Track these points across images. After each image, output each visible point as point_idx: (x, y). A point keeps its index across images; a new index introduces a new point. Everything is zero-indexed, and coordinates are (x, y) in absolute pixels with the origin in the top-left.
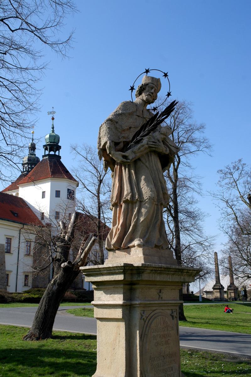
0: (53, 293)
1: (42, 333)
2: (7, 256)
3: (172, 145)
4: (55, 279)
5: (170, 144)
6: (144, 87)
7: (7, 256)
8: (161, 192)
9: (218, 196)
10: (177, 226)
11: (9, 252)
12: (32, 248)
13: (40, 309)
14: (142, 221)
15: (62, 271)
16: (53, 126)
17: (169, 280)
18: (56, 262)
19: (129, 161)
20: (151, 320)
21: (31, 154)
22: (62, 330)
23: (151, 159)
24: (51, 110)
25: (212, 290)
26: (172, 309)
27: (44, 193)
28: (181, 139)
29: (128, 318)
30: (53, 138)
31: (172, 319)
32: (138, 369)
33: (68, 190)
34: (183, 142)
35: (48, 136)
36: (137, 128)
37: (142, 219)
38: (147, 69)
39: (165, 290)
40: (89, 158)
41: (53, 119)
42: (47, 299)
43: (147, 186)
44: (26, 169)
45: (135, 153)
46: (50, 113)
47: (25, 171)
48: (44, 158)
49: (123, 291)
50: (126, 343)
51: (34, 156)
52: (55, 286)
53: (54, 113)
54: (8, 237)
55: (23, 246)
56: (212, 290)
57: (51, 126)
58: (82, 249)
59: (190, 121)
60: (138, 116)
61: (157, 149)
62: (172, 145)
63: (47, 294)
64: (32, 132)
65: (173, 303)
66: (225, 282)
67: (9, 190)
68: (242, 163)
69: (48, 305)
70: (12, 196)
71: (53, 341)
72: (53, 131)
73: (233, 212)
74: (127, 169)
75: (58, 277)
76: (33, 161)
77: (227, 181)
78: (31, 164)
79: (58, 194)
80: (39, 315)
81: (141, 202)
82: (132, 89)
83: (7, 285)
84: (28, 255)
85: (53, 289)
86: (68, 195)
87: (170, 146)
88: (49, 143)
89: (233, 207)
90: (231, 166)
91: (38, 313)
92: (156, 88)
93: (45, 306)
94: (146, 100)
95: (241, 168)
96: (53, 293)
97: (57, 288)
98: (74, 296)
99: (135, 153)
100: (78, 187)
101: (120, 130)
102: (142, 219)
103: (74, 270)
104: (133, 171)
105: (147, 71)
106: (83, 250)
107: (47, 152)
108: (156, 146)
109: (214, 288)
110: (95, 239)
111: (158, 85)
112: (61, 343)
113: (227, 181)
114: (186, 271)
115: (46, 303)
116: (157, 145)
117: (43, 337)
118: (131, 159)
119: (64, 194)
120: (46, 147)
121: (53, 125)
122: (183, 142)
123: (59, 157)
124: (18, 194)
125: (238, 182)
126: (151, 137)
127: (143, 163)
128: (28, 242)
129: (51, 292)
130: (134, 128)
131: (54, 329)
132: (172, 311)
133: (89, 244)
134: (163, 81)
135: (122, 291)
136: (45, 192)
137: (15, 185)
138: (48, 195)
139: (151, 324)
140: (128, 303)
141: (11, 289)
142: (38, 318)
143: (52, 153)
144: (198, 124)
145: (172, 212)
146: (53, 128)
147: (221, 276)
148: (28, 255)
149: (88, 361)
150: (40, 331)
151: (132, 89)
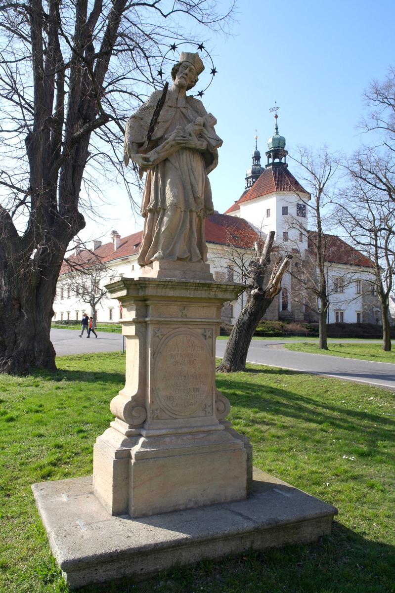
0: (244, 324)
3: (211, 137)
5: (209, 136)
6: (176, 68)
8: (191, 197)
13: (231, 340)
14: (163, 232)
15: (252, 299)
16: (277, 126)
17: (189, 296)
19: (151, 163)
21: (255, 165)
22: (255, 363)
23: (183, 157)
24: (273, 105)
27: (268, 210)
29: (141, 334)
30: (277, 142)
31: (204, 339)
32: (149, 386)
35: (271, 140)
36: (168, 121)
37: (163, 229)
38: (173, 45)
40: (305, 162)
41: (276, 117)
43: (171, 191)
44: (250, 183)
45: (158, 153)
46: (272, 110)
47: (249, 187)
49: (136, 307)
50: (139, 360)
51: (259, 167)
53: (277, 109)
57: (275, 127)
58: (274, 273)
60: (170, 107)
61: (187, 145)
62: (212, 137)
64: (255, 137)
69: (238, 336)
72: (277, 133)
74: (155, 173)
76: (256, 174)
78: (256, 177)
79: (285, 210)
81: (164, 210)
85: (244, 318)
86: (297, 211)
87: (208, 139)
88: (272, 149)
92: (193, 67)
93: (236, 337)
94: (179, 84)
98: (305, 330)
99: (158, 153)
100: (310, 199)
101: (145, 128)
102: (163, 229)
103: (265, 297)
104: (159, 175)
106: (275, 274)
107: (271, 161)
108: (185, 141)
110: (287, 261)
111: (195, 62)
114: (216, 286)
115: (237, 334)
116: (187, 140)
118: (152, 161)
119: (292, 211)
120: (269, 154)
121: (277, 125)
123: (285, 165)
126: (180, 131)
127: (172, 164)
130: (163, 122)
131: (247, 361)
132: (205, 330)
133: (281, 267)
134: (202, 54)
135: (135, 307)
136: (269, 209)
138: (273, 213)
140: (141, 320)
143: (277, 160)
146: (277, 129)
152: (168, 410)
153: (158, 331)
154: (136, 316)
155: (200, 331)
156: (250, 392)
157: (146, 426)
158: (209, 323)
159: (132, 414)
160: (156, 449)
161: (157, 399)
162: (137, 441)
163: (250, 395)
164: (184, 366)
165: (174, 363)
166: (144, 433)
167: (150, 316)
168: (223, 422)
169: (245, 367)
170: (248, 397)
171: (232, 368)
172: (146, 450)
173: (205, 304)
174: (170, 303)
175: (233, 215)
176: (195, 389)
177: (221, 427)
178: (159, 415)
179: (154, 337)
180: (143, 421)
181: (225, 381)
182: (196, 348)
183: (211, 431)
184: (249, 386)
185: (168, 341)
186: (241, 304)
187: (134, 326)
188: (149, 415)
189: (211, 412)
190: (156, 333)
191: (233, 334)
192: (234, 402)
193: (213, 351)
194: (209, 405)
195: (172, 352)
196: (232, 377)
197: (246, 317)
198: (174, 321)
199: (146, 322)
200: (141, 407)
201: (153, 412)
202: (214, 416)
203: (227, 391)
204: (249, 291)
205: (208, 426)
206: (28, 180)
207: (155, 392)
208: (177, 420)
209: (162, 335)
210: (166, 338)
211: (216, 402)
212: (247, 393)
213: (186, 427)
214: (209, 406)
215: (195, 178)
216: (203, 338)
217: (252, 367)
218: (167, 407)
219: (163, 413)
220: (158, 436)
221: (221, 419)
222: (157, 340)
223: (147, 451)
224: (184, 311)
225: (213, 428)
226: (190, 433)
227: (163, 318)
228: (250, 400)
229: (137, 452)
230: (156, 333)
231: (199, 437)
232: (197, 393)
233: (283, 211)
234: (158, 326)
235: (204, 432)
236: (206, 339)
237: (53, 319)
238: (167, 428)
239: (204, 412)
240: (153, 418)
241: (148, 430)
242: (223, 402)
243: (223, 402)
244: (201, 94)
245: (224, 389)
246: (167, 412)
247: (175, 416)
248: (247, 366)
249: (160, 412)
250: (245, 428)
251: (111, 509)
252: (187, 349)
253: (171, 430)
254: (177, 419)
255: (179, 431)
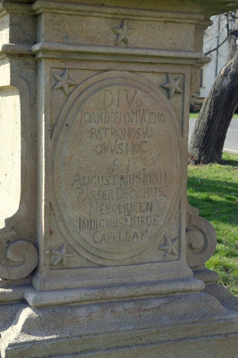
0: (223, 91)
1: (204, 154)
4: (227, 68)
18: (232, 36)
20: (84, 95)
26: (166, 73)
31: (164, 98)
32: (43, 198)
39: (142, 23)
42: (213, 100)
52: (227, 78)
63: (213, 93)
65: (168, 57)
71: (220, 168)
75: (231, 63)
80: (200, 126)
83: (201, 86)
85: (223, 84)
91: (198, 123)
93: (210, 112)
96: (222, 91)
97: (231, 82)
112: (232, 172)
115: (211, 107)
117: (205, 161)
129: (219, 90)
131: (225, 149)
132: (167, 77)
135: (7, 18)
139: (83, 102)
140: (22, 48)
142: (198, 132)
149: (228, 198)
150: (201, 151)
152: (83, 248)
153: (62, 76)
154: (11, 40)
155: (157, 79)
156: (233, 197)
157: (37, 282)
158: (177, 62)
159: (6, 256)
160: (54, 336)
161: (60, 225)
162: (15, 315)
163: (234, 202)
164: (118, 156)
165: (99, 150)
166: (30, 297)
167: (42, 39)
168: (202, 271)
169: (220, 157)
170: (231, 205)
171: (202, 158)
172: (33, 338)
173: (168, 15)
174: (88, 8)
176: (144, 207)
177: (198, 284)
178: (65, 259)
179: (52, 89)
180: (31, 271)
181: (193, 178)
182: (147, 117)
183: (175, 292)
184: (230, 188)
185: (86, 99)
186: (214, 67)
187: (8, 65)
188: (43, 259)
189: (176, 252)
190: (57, 81)
191: (205, 110)
192: (208, 213)
193: (185, 123)
194: (173, 237)
195: (94, 125)
196: (200, 172)
197: (227, 82)
198: (98, 54)
199: (33, 55)
200: (26, 243)
201: (51, 254)
202: (183, 259)
203: (196, 195)
204: (233, 40)
205: (170, 281)
207: (56, 212)
208: (104, 270)
209: (70, 85)
210: (81, 93)
211: (187, 231)
212: (228, 198)
213: (123, 285)
214: (173, 240)
215: (153, 72)
216: (162, 94)
217: (232, 158)
218: (81, 243)
219: (75, 254)
220: (61, 305)
221: (197, 267)
222: (61, 95)
223: (34, 342)
224: (120, 31)
225: (181, 286)
226: (131, 299)
227: (72, 44)
228: (234, 209)
229: (10, 346)
230: (57, 81)
231: (148, 307)
232: (148, 213)
234: (63, 65)
235: (161, 295)
236: (169, 98)
238: (82, 288)
239: (163, 252)
240: (51, 265)
241: (42, 291)
242: (201, 230)
243: (201, 230)
245: (192, 192)
246: (83, 253)
247: (99, 262)
248: (224, 157)
249: (68, 252)
250: (229, 259)
252: (127, 118)
253: (88, 293)
254: (103, 266)
255: (109, 293)
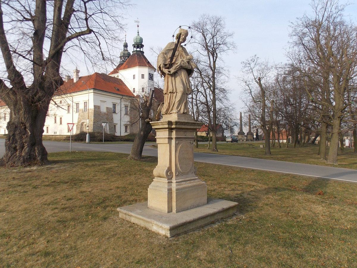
2: (114, 115)
7: (114, 115)
9: (241, 79)
10: (214, 97)
11: (114, 112)
12: (128, 109)
25: (237, 135)
27: (134, 76)
28: (219, 42)
33: (149, 74)
34: (220, 44)
46: (136, 22)
48: (134, 53)
54: (114, 103)
55: (124, 109)
56: (237, 135)
59: (225, 30)
66: (246, 130)
67: (112, 74)
68: (256, 57)
70: (114, 77)
73: (249, 89)
77: (247, 69)
79: (143, 76)
82: (173, 36)
84: (126, 114)
89: (249, 85)
90: (250, 59)
95: (256, 60)
105: (180, 27)
107: (135, 49)
109: (238, 134)
113: (247, 69)
119: (147, 77)
121: (138, 30)
122: (220, 44)
123: (143, 52)
124: (118, 76)
125: (253, 70)
128: (126, 107)
137: (116, 71)
141: (118, 134)
143: (138, 49)
144: (230, 32)
145: (212, 89)
146: (138, 33)
147: (243, 126)
148: (126, 114)
151: (173, 36)
175: (113, 76)
206: (106, 73)
216: (190, 144)
233: (142, 76)
237: (43, 134)
244: (185, 45)
251: (167, 210)
